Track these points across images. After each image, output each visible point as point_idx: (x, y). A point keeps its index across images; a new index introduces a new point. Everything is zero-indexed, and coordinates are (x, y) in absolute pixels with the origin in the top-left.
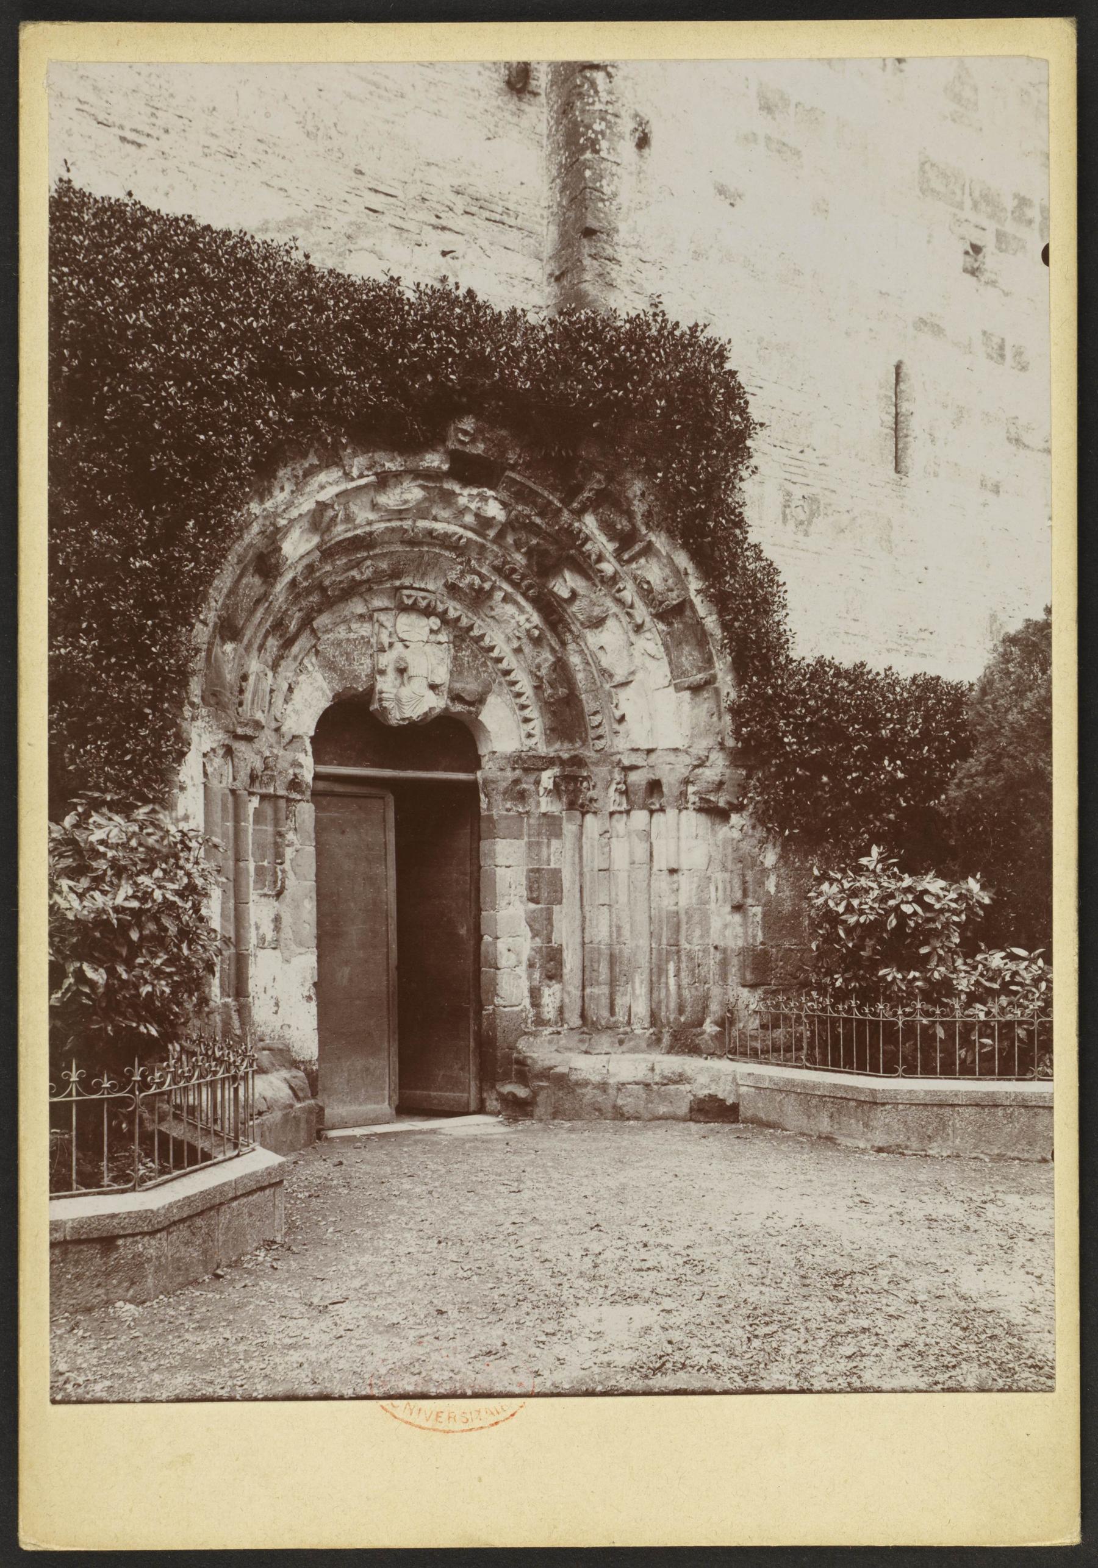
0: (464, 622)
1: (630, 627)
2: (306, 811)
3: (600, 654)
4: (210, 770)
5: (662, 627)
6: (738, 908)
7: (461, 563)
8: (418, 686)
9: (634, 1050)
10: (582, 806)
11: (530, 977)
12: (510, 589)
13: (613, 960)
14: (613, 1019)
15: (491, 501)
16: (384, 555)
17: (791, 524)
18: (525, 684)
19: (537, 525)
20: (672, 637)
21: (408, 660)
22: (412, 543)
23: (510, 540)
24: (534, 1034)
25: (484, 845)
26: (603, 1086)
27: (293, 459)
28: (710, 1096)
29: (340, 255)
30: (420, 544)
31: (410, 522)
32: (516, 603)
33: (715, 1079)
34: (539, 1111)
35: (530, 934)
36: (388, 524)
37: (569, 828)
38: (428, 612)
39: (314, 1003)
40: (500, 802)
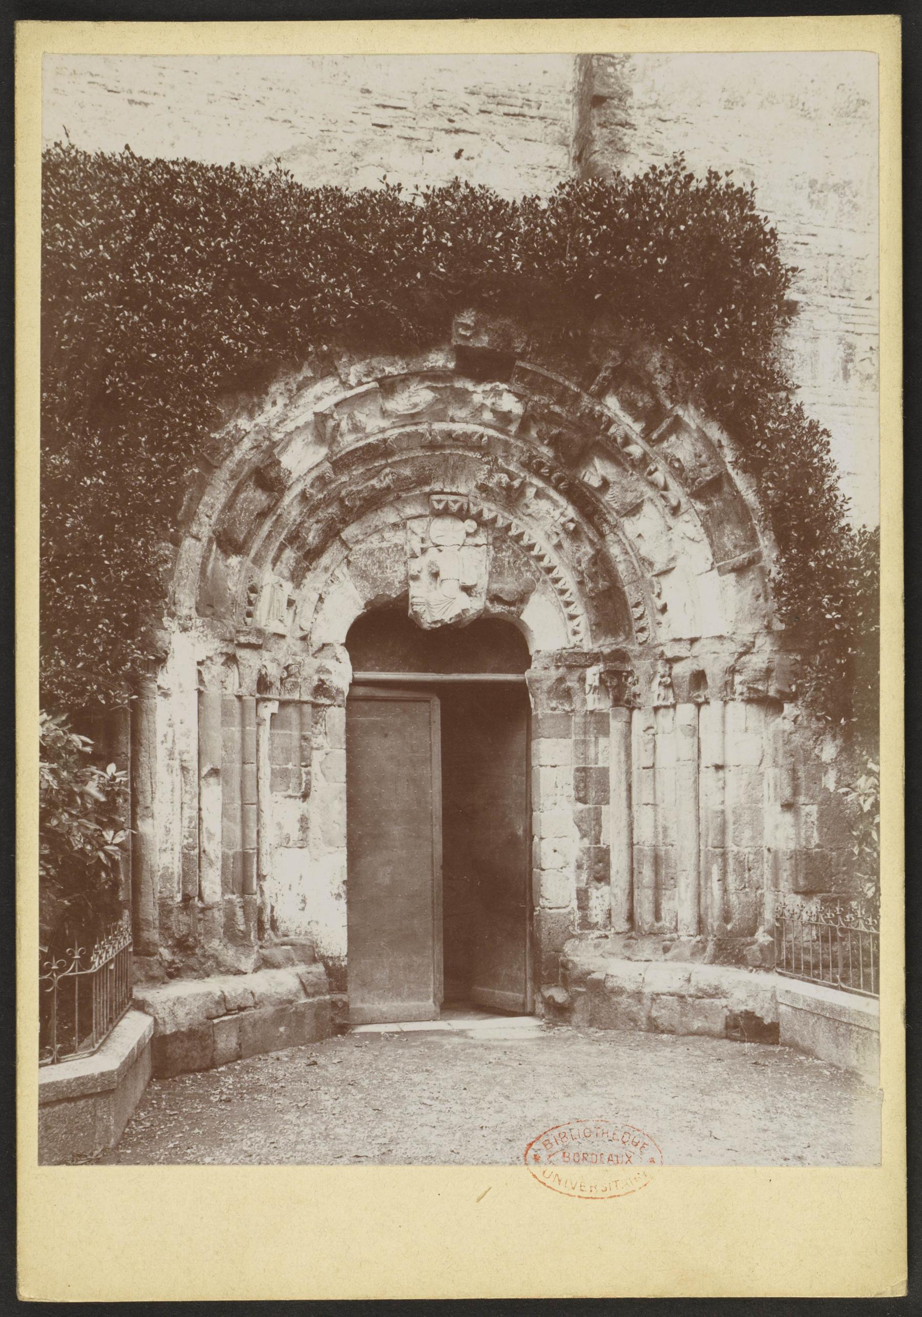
0: (500, 523)
1: (667, 510)
2: (336, 716)
3: (638, 543)
4: (206, 677)
5: (700, 506)
6: (789, 807)
7: (487, 463)
8: (450, 588)
9: (677, 958)
10: (628, 702)
11: (578, 879)
12: (541, 484)
13: (657, 861)
14: (657, 925)
15: (505, 394)
16: (406, 461)
17: (854, 380)
18: (569, 581)
19: (559, 415)
20: (712, 516)
21: (438, 563)
22: (432, 446)
23: (533, 433)
24: (580, 938)
25: (534, 745)
26: (638, 995)
27: (285, 374)
28: (747, 1012)
29: (346, 174)
30: (442, 447)
31: (425, 426)
32: (549, 498)
33: (753, 996)
34: (576, 1018)
35: (578, 835)
36: (402, 430)
37: (616, 726)
38: (462, 515)
39: (343, 902)
40: (545, 702)
